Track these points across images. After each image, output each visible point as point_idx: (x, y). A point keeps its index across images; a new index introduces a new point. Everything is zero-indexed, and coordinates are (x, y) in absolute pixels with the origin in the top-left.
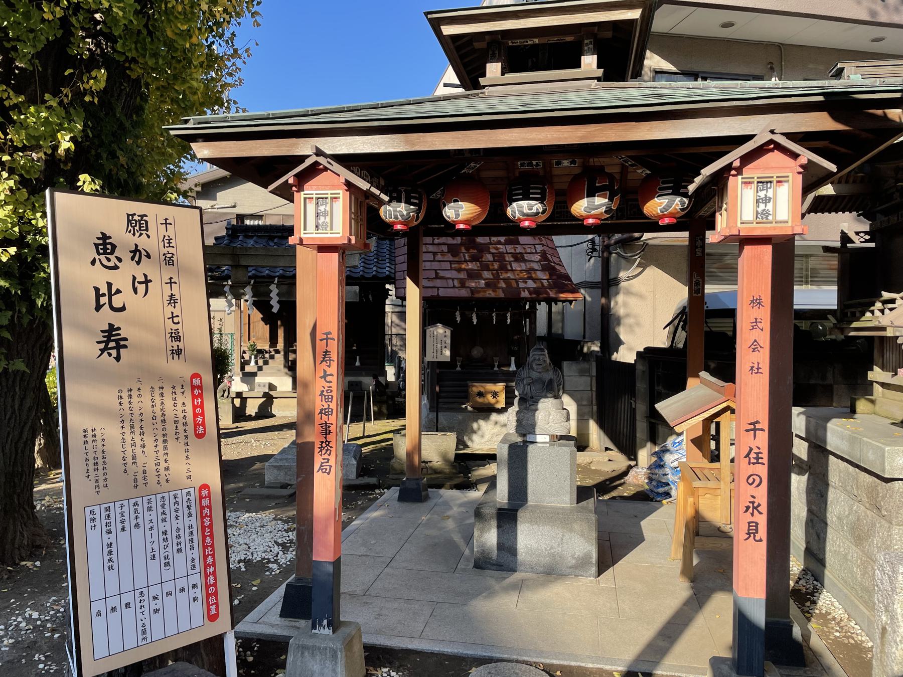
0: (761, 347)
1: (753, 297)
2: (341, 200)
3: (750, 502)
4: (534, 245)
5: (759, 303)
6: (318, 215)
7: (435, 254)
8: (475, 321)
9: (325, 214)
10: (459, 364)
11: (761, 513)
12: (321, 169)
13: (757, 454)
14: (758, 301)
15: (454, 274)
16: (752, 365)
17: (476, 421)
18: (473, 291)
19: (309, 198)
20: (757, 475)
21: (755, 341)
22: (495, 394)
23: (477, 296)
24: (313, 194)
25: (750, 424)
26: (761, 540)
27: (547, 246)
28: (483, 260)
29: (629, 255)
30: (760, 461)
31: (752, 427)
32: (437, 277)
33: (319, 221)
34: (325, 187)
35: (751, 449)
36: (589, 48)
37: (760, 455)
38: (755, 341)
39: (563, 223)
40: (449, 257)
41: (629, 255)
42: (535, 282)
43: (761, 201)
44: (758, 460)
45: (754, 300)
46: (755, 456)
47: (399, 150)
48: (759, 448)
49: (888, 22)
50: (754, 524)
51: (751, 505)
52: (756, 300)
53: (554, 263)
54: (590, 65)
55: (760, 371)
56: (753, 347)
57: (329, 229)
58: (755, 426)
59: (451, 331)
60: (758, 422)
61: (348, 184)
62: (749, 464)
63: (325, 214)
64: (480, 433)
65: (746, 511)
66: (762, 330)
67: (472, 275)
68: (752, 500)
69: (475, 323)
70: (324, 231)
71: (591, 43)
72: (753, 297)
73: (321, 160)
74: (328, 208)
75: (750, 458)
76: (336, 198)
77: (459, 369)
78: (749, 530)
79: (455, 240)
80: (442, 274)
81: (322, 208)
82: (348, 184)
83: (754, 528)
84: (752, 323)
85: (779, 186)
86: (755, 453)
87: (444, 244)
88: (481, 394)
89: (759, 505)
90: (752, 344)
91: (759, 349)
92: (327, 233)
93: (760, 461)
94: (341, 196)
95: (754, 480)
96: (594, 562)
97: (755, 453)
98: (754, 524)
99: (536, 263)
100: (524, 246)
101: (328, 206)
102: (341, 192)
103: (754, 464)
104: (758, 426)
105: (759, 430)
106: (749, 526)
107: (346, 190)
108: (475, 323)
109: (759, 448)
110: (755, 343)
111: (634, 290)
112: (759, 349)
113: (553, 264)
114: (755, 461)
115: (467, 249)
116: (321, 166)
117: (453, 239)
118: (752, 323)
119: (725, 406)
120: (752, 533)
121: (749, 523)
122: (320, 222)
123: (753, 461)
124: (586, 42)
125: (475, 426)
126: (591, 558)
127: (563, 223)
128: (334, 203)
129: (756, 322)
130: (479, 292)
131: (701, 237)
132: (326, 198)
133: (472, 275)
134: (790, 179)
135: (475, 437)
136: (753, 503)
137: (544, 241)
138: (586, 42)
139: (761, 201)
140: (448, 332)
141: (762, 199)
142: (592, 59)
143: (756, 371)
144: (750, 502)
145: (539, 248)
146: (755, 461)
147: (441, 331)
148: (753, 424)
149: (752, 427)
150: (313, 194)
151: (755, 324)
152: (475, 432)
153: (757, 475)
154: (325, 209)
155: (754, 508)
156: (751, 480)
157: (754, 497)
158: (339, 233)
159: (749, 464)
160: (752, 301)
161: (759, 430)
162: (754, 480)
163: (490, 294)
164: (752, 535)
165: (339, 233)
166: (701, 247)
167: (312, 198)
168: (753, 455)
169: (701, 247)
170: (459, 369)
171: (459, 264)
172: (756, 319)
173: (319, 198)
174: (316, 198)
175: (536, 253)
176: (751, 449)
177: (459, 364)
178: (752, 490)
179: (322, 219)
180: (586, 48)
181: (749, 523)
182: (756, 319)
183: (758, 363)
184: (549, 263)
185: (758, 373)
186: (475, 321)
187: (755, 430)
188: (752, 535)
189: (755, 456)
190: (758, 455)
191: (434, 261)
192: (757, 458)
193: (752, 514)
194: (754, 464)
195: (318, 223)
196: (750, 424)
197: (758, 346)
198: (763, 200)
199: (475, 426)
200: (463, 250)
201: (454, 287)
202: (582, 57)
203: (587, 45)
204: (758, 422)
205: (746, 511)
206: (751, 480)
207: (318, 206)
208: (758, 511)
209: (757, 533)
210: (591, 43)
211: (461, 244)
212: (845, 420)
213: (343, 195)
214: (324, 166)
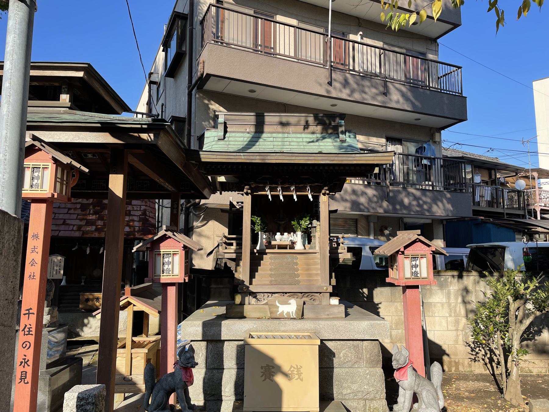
0: (36, 263)
1: (34, 233)
2: (50, 169)
3: (23, 359)
4: (140, 205)
5: (37, 237)
6: (33, 179)
7: (69, 209)
8: (88, 252)
9: (38, 178)
10: (83, 281)
11: (29, 366)
12: (36, 149)
13: (29, 328)
14: (36, 236)
15: (78, 222)
16: (30, 274)
17: (87, 318)
18: (84, 233)
19: (28, 167)
20: (28, 342)
21: (33, 259)
22: (98, 299)
23: (85, 236)
24: (40, 165)
25: (26, 310)
26: (28, 383)
27: (150, 207)
28: (102, 214)
29: (197, 213)
30: (31, 333)
31: (27, 312)
32: (64, 223)
33: (33, 183)
34: (37, 160)
35: (26, 326)
36: (65, 90)
37: (31, 329)
38: (33, 259)
39: (98, 191)
40: (79, 211)
41: (197, 213)
42: (130, 228)
43: (35, 178)
44: (29, 333)
45: (34, 235)
46: (28, 330)
47: (100, 142)
48: (30, 325)
49: (402, 108)
50: (25, 373)
51: (23, 361)
52: (35, 235)
53: (149, 217)
54: (65, 100)
55: (34, 277)
56: (32, 263)
57: (39, 187)
58: (29, 311)
59: (65, 259)
60: (31, 309)
61: (55, 161)
62: (24, 335)
63: (38, 178)
64: (89, 326)
65: (20, 365)
66: (37, 253)
67: (90, 223)
68: (25, 357)
69: (100, 253)
70: (37, 189)
71: (66, 88)
72: (34, 233)
73: (37, 143)
74: (40, 175)
75: (25, 331)
76: (46, 168)
77: (83, 284)
78: (21, 376)
79: (88, 201)
80: (68, 222)
81: (36, 174)
82: (55, 161)
83: (24, 375)
84: (32, 249)
85: (46, 170)
86: (28, 328)
87: (79, 203)
88: (88, 300)
89: (28, 361)
90: (31, 262)
91: (35, 264)
92: (38, 190)
93: (31, 333)
94: (50, 167)
95: (26, 345)
96: (47, 407)
97: (28, 328)
98: (25, 373)
99: (136, 217)
100: (133, 206)
101: (41, 173)
102: (50, 164)
103: (27, 335)
104: (31, 312)
105: (31, 313)
106: (22, 374)
107: (54, 163)
108: (100, 253)
109: (30, 325)
110: (33, 261)
111: (203, 233)
112: (35, 264)
113: (148, 218)
114: (28, 333)
115: (94, 207)
116: (37, 148)
117: (87, 200)
118: (32, 249)
119: (126, 301)
120: (23, 379)
121: (22, 372)
122: (34, 183)
123: (26, 333)
124: (63, 87)
125: (86, 321)
126: (45, 405)
127: (98, 191)
128: (45, 171)
129: (34, 248)
130: (87, 234)
131: (176, 202)
132: (40, 168)
133: (90, 223)
134: (50, 167)
135: (85, 329)
136: (25, 359)
137: (148, 204)
138: (63, 87)
139: (35, 178)
140: (64, 259)
141: (36, 177)
142: (67, 96)
143: (32, 278)
144: (23, 359)
145: (143, 208)
146: (28, 333)
147: (58, 259)
148: (28, 310)
149: (27, 312)
150: (30, 165)
151: (34, 249)
152: (86, 325)
153: (28, 342)
154: (38, 175)
155: (25, 362)
156: (24, 345)
157: (25, 356)
158: (46, 191)
159: (24, 335)
160: (33, 236)
161: (31, 313)
162: (26, 345)
163: (95, 235)
164: (23, 380)
165: (46, 191)
166: (176, 208)
167: (30, 167)
168: (27, 329)
169: (176, 208)
170: (83, 284)
171: (84, 216)
172: (35, 246)
173: (34, 168)
174: (32, 167)
175: (140, 210)
176: (26, 326)
177: (83, 281)
178: (25, 351)
179: (35, 181)
180: (63, 90)
181: (22, 372)
182: (35, 246)
183: (34, 273)
184: (145, 217)
185: (33, 279)
186: (88, 252)
187: (29, 314)
188: (23, 380)
189: (28, 330)
190: (29, 329)
191: (67, 213)
192: (29, 331)
193: (24, 367)
194: (27, 335)
195: (32, 184)
196: (26, 310)
197: (34, 263)
198: (36, 178)
199: (86, 321)
200: (91, 207)
201: (72, 230)
202: (61, 95)
203: (64, 88)
204: (31, 309)
205: (20, 365)
206: (24, 345)
207: (33, 173)
208: (27, 364)
209: (26, 378)
210: (66, 88)
211: (92, 204)
212: (214, 307)
213: (51, 166)
214: (38, 147)
